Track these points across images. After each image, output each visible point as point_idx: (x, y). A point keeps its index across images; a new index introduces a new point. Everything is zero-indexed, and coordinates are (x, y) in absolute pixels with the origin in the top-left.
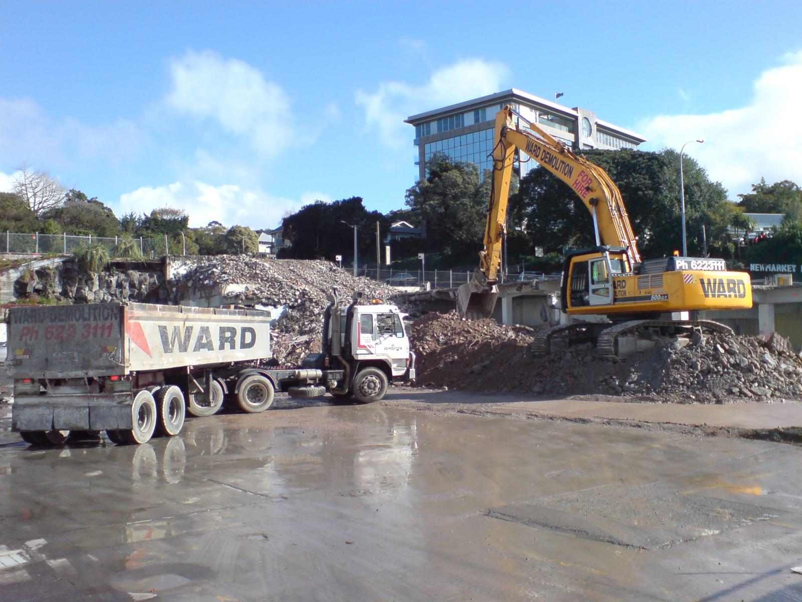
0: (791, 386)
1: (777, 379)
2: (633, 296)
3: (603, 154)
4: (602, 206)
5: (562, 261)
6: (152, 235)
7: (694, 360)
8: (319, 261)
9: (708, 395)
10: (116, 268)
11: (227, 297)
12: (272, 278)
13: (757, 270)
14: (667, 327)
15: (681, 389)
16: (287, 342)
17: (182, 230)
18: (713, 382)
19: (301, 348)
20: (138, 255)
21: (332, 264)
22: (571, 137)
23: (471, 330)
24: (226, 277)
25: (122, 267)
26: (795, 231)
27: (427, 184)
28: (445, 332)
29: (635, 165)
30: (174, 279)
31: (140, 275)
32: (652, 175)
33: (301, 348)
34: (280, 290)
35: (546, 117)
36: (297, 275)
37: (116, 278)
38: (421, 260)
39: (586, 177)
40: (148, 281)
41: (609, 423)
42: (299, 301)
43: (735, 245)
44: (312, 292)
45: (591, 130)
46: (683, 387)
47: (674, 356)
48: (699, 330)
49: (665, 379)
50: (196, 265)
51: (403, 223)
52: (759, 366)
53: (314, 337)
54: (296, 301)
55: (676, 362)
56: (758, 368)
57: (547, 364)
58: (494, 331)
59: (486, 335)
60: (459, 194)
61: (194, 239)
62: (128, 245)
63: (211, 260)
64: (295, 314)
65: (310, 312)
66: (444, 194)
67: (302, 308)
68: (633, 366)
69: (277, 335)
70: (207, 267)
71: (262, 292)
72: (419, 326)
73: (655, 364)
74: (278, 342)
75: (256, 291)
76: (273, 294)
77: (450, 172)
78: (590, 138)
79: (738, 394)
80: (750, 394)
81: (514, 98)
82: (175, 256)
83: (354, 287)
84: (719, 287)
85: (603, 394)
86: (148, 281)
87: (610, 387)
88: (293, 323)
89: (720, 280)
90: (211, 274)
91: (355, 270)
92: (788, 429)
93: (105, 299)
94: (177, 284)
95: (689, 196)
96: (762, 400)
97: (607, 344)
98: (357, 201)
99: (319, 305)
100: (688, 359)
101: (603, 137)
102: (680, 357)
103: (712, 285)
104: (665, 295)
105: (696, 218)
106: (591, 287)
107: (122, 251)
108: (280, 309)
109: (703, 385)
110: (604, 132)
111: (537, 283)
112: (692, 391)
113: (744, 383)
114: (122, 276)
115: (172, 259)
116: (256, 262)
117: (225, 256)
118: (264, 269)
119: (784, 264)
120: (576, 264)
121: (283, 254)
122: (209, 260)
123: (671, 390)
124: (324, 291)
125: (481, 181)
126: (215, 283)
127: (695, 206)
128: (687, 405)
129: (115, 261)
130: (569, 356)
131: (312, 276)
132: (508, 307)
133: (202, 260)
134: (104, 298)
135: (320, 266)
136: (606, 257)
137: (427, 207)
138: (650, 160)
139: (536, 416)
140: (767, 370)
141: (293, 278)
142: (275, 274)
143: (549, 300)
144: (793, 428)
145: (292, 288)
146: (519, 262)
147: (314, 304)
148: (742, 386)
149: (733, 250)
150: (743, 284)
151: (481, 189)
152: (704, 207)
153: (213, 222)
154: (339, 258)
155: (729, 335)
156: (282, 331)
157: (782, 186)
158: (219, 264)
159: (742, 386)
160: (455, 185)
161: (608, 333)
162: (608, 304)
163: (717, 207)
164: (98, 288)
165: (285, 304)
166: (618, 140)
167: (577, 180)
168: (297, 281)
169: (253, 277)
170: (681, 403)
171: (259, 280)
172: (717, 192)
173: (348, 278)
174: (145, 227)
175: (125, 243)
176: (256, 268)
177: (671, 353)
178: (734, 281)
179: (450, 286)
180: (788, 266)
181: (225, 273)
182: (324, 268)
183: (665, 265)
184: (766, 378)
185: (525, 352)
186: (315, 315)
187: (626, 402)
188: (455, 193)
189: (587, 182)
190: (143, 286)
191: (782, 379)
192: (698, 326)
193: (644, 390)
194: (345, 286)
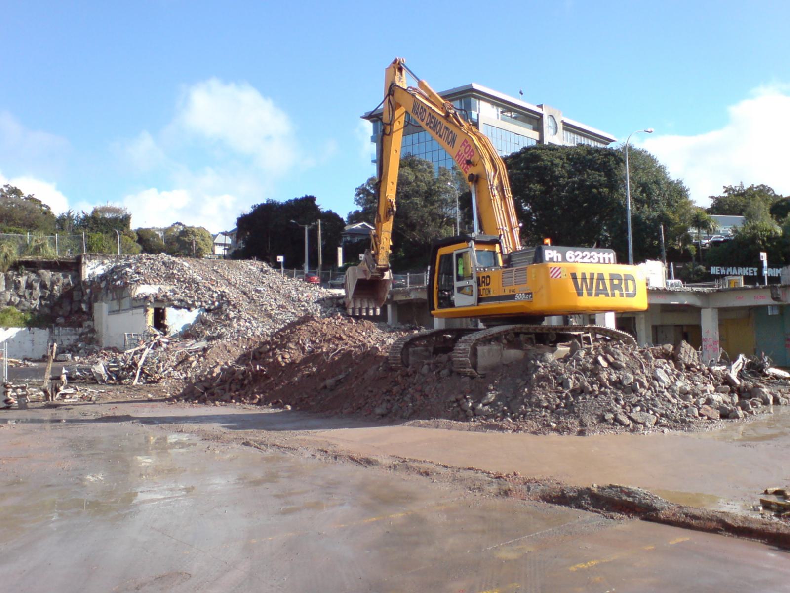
0: (685, 410)
1: (669, 401)
2: (498, 295)
3: (557, 149)
4: (482, 182)
7: (565, 376)
10: (25, 267)
11: (136, 299)
12: (190, 278)
14: (547, 334)
15: (544, 413)
20: (52, 253)
21: (264, 264)
22: (536, 135)
23: (344, 337)
25: (31, 266)
26: (756, 231)
28: (314, 339)
29: (591, 160)
30: (88, 280)
31: (53, 275)
32: (609, 174)
33: (195, 355)
35: (509, 114)
37: (25, 278)
39: (468, 148)
40: (61, 282)
42: (217, 304)
43: (696, 247)
44: (231, 294)
45: (557, 128)
46: (546, 412)
48: (589, 337)
49: (525, 400)
51: (364, 225)
52: (646, 384)
54: (213, 303)
55: (544, 378)
56: (644, 387)
57: (400, 379)
60: (411, 192)
62: (40, 243)
64: (210, 318)
65: (226, 316)
67: (217, 311)
68: (493, 383)
69: (167, 341)
72: (285, 332)
73: (519, 380)
74: (168, 349)
76: (188, 296)
78: (556, 137)
80: (627, 421)
81: (474, 94)
82: (91, 255)
84: (598, 284)
86: (61, 282)
89: (599, 274)
93: (13, 300)
94: (91, 285)
97: (463, 355)
98: (311, 199)
101: (570, 136)
102: (549, 371)
103: (588, 281)
104: (529, 294)
106: (457, 284)
107: (32, 249)
108: (195, 313)
110: (571, 131)
113: (623, 407)
114: (33, 276)
116: (174, 261)
118: (183, 269)
119: (745, 267)
120: (442, 256)
123: (531, 415)
124: (245, 293)
126: (126, 284)
129: (24, 260)
130: (425, 369)
134: (11, 299)
135: (250, 267)
136: (471, 247)
138: (606, 155)
144: (611, 487)
145: (210, 289)
147: (231, 307)
149: (694, 252)
150: (633, 280)
153: (177, 223)
154: (281, 259)
155: (617, 344)
161: (465, 342)
162: (472, 305)
163: (677, 206)
164: (4, 289)
165: (201, 306)
166: (586, 139)
167: (460, 150)
169: (169, 278)
170: (534, 433)
171: (176, 281)
172: (678, 192)
174: (83, 226)
175: (36, 241)
176: (173, 267)
177: (539, 367)
178: (620, 276)
180: (750, 269)
182: (254, 269)
183: (532, 256)
184: (652, 400)
185: (381, 364)
189: (470, 154)
190: (56, 287)
191: (674, 401)
192: (587, 333)
193: (499, 414)
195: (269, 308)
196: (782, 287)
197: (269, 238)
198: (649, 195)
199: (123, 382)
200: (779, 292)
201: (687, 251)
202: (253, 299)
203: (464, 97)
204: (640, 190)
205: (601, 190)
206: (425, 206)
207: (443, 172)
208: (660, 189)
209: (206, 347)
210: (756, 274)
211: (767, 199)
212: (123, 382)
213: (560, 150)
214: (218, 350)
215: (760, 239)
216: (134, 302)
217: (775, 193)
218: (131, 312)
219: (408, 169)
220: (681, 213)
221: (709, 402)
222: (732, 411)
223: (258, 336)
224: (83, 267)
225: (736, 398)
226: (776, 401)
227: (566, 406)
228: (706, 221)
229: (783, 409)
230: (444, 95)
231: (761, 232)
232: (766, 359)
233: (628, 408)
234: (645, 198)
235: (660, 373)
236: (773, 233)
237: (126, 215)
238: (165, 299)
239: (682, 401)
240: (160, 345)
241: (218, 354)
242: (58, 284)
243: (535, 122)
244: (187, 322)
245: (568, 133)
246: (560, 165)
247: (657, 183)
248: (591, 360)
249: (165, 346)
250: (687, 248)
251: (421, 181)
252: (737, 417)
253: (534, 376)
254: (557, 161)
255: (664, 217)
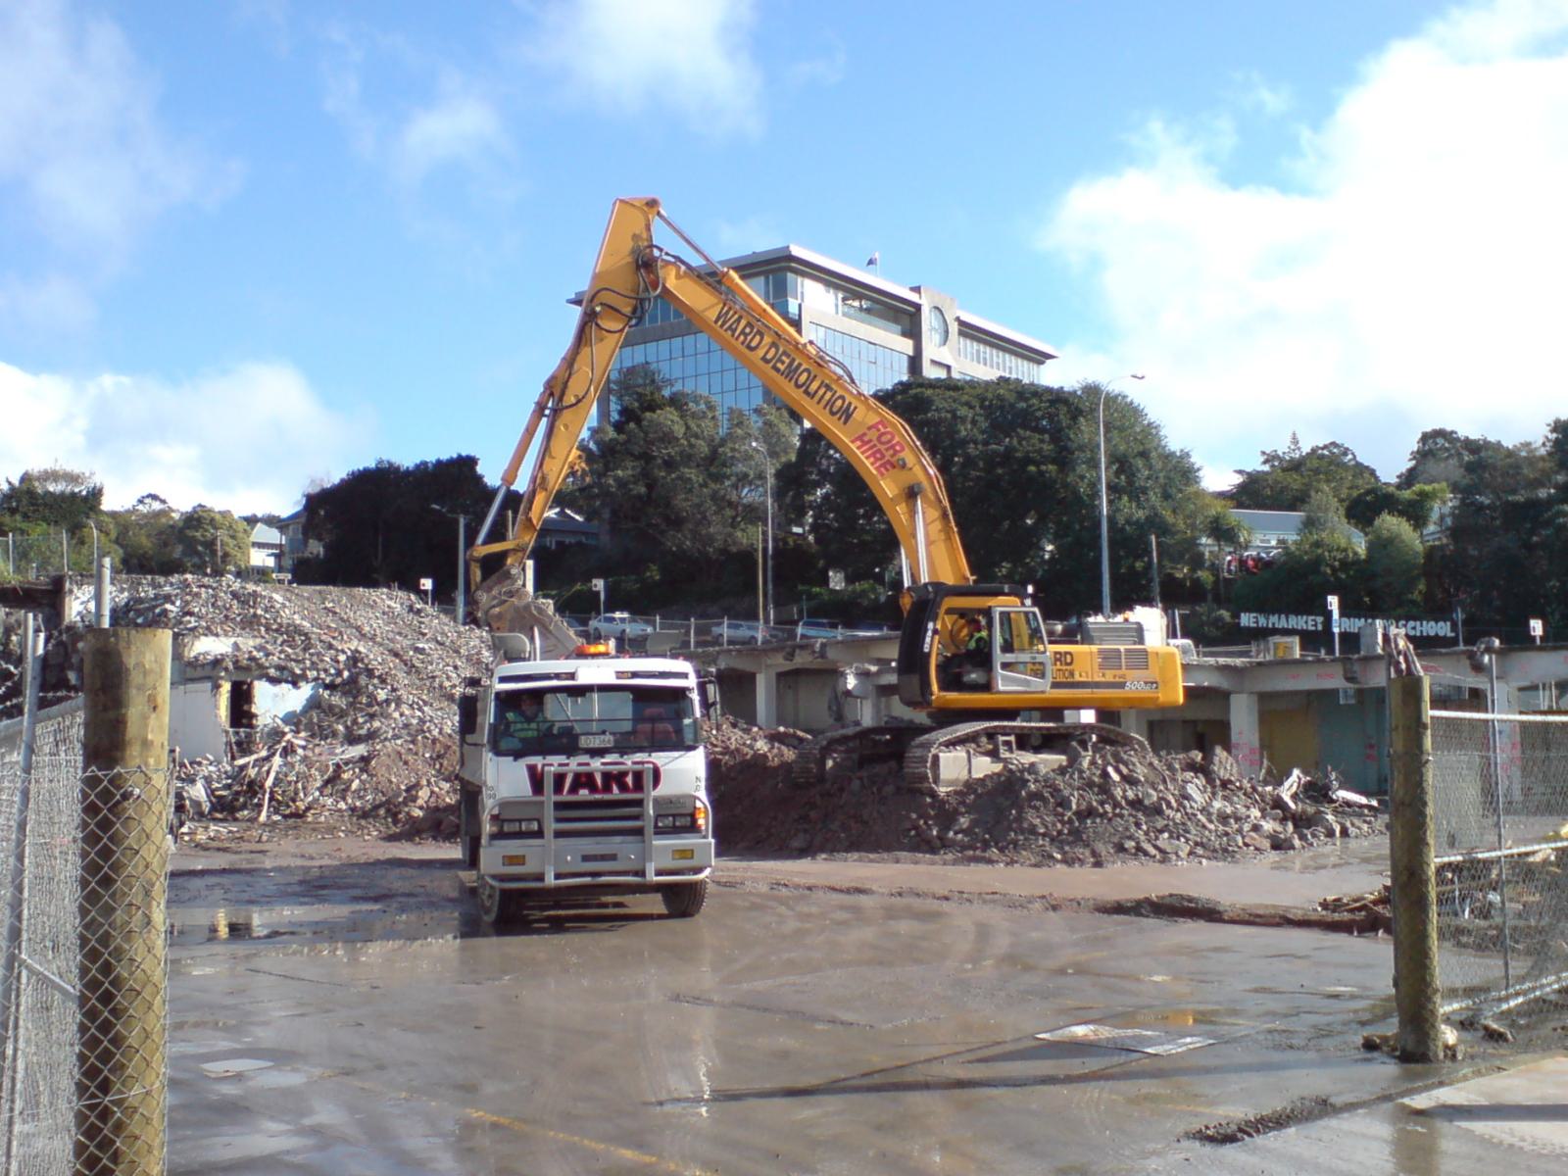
0: (1225, 839)
1: (1204, 827)
3: (962, 388)
5: (883, 599)
6: (24, 526)
8: (385, 590)
9: (1083, 854)
12: (289, 625)
13: (1253, 625)
14: (1029, 736)
15: (1041, 842)
16: (323, 758)
17: (88, 518)
18: (1094, 832)
19: (353, 769)
21: (413, 597)
24: (192, 622)
27: (611, 433)
31: (7, 614)
32: (1057, 435)
33: (353, 769)
34: (305, 650)
35: (856, 304)
36: (342, 619)
38: (598, 593)
41: (900, 894)
42: (346, 674)
44: (372, 657)
45: (947, 332)
47: (1033, 786)
50: (126, 594)
53: (378, 747)
54: (339, 673)
55: (1037, 795)
56: (1171, 808)
58: (729, 739)
59: (716, 746)
61: (113, 535)
63: (160, 586)
64: (338, 700)
65: (368, 697)
66: (646, 457)
67: (351, 687)
69: (303, 743)
70: (152, 599)
71: (267, 655)
75: (255, 653)
76: (292, 660)
77: (659, 412)
78: (945, 349)
79: (1133, 851)
80: (1153, 851)
81: (793, 265)
82: (82, 575)
83: (460, 647)
85: (909, 851)
87: (923, 840)
88: (333, 719)
90: (159, 615)
91: (461, 610)
92: (1163, 897)
95: (1127, 477)
96: (1170, 860)
98: (466, 464)
99: (387, 684)
100: (1056, 790)
101: (973, 347)
105: (1138, 520)
108: (306, 690)
109: (1077, 836)
110: (973, 338)
111: (823, 645)
112: (1058, 847)
113: (1146, 833)
115: (77, 583)
116: (255, 592)
117: (189, 577)
118: (272, 607)
121: (305, 572)
122: (155, 585)
124: (396, 655)
125: (722, 432)
127: (1139, 498)
128: (1045, 869)
130: (856, 784)
131: (372, 622)
132: (767, 688)
133: (140, 584)
137: (611, 482)
138: (1052, 402)
139: (786, 885)
140: (1189, 811)
141: (333, 625)
142: (296, 617)
143: (841, 680)
144: (1171, 895)
145: (330, 647)
146: (797, 600)
147: (376, 681)
148: (1143, 838)
151: (721, 450)
152: (1154, 498)
154: (427, 584)
156: (313, 736)
157: (1326, 452)
158: (176, 595)
159: (1143, 838)
160: (668, 438)
165: (316, 679)
168: (341, 633)
169: (250, 623)
170: (1035, 865)
171: (263, 629)
172: (1182, 471)
173: (446, 628)
174: (9, 509)
177: (1028, 781)
179: (689, 647)
181: (191, 614)
185: (780, 778)
186: (378, 704)
187: (945, 864)
188: (669, 454)
190: (14, 638)
191: (1212, 827)
194: (441, 644)
195: (447, 684)
196: (1359, 659)
197: (380, 539)
198: (1130, 483)
199: (238, 815)
200: (1356, 667)
201: (1197, 582)
202: (413, 666)
203: (773, 271)
204: (1114, 467)
205: (1043, 468)
206: (705, 485)
207: (737, 419)
208: (1150, 468)
209: (366, 754)
210: (1320, 628)
211: (1341, 478)
212: (238, 815)
213: (967, 389)
214: (388, 762)
215: (1327, 565)
216: (188, 669)
217: (1358, 459)
218: (182, 687)
219: (671, 413)
220: (1188, 512)
221: (1256, 828)
222: (1285, 840)
223: (450, 736)
224: (67, 599)
225: (1290, 827)
226: (1345, 833)
227: (1070, 833)
228: (1233, 529)
229: (1353, 844)
230: (737, 264)
231: (1329, 552)
232: (1333, 776)
233: (1152, 834)
234: (1124, 484)
235: (1191, 789)
236: (1351, 555)
237: (94, 488)
238: (253, 664)
239: (1221, 828)
240: (294, 752)
241: (389, 768)
242: (19, 632)
243: (906, 320)
244: (291, 709)
245: (968, 342)
246: (969, 419)
247: (1144, 455)
248: (1098, 772)
249: (300, 751)
250: (1198, 578)
251: (696, 436)
252: (1292, 847)
253: (1023, 793)
254: (963, 411)
255: (1157, 520)
